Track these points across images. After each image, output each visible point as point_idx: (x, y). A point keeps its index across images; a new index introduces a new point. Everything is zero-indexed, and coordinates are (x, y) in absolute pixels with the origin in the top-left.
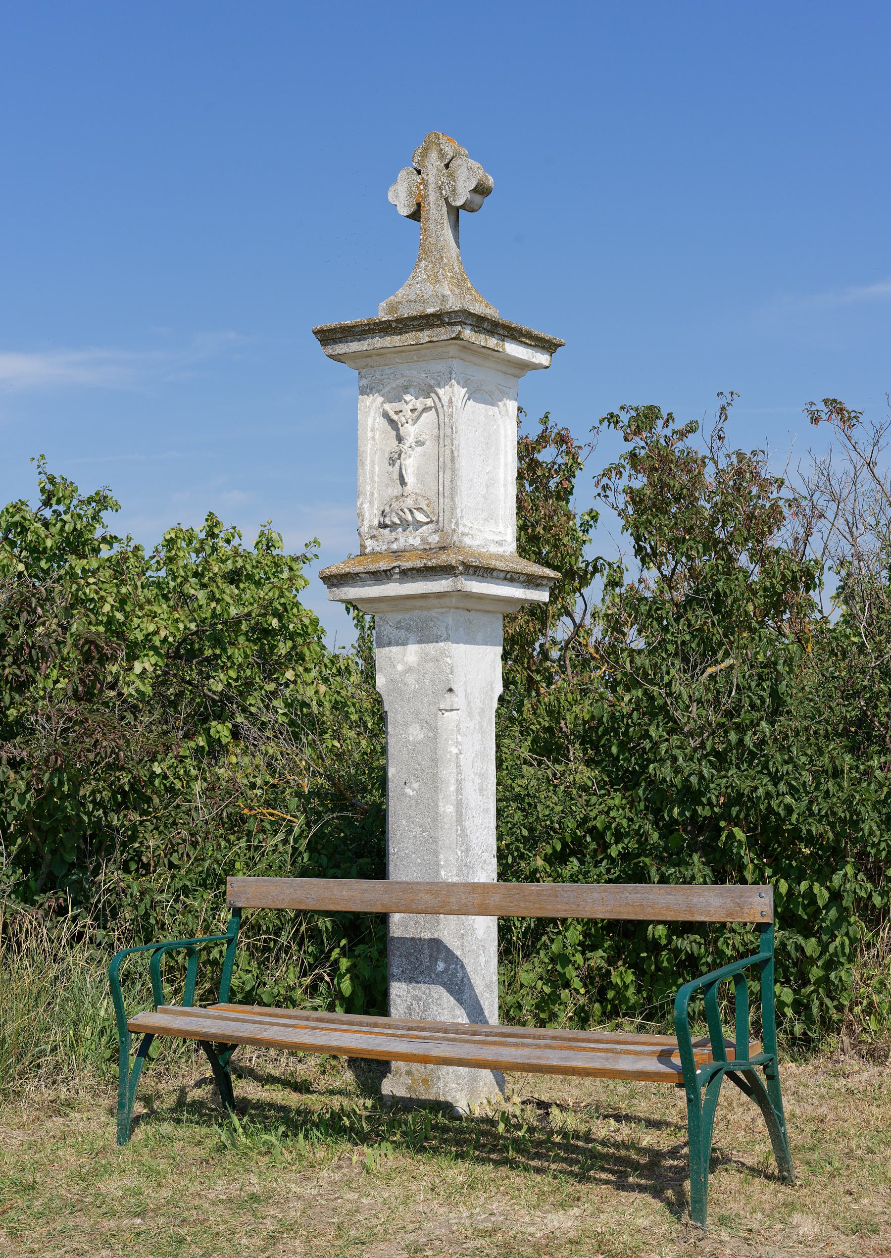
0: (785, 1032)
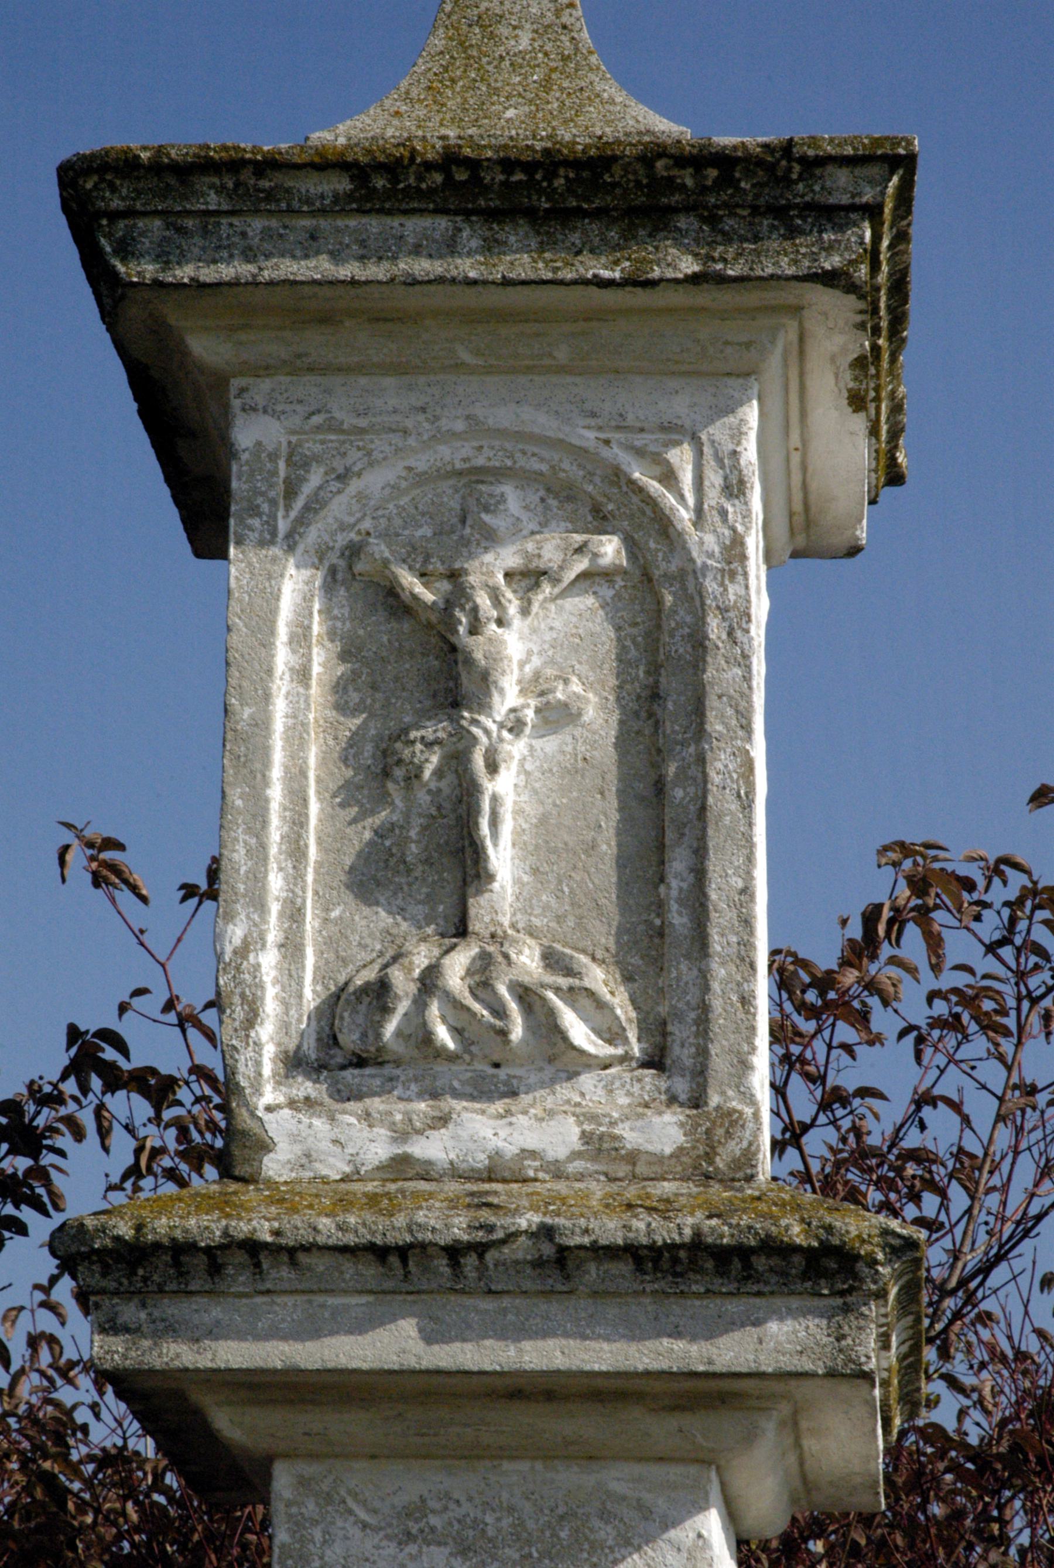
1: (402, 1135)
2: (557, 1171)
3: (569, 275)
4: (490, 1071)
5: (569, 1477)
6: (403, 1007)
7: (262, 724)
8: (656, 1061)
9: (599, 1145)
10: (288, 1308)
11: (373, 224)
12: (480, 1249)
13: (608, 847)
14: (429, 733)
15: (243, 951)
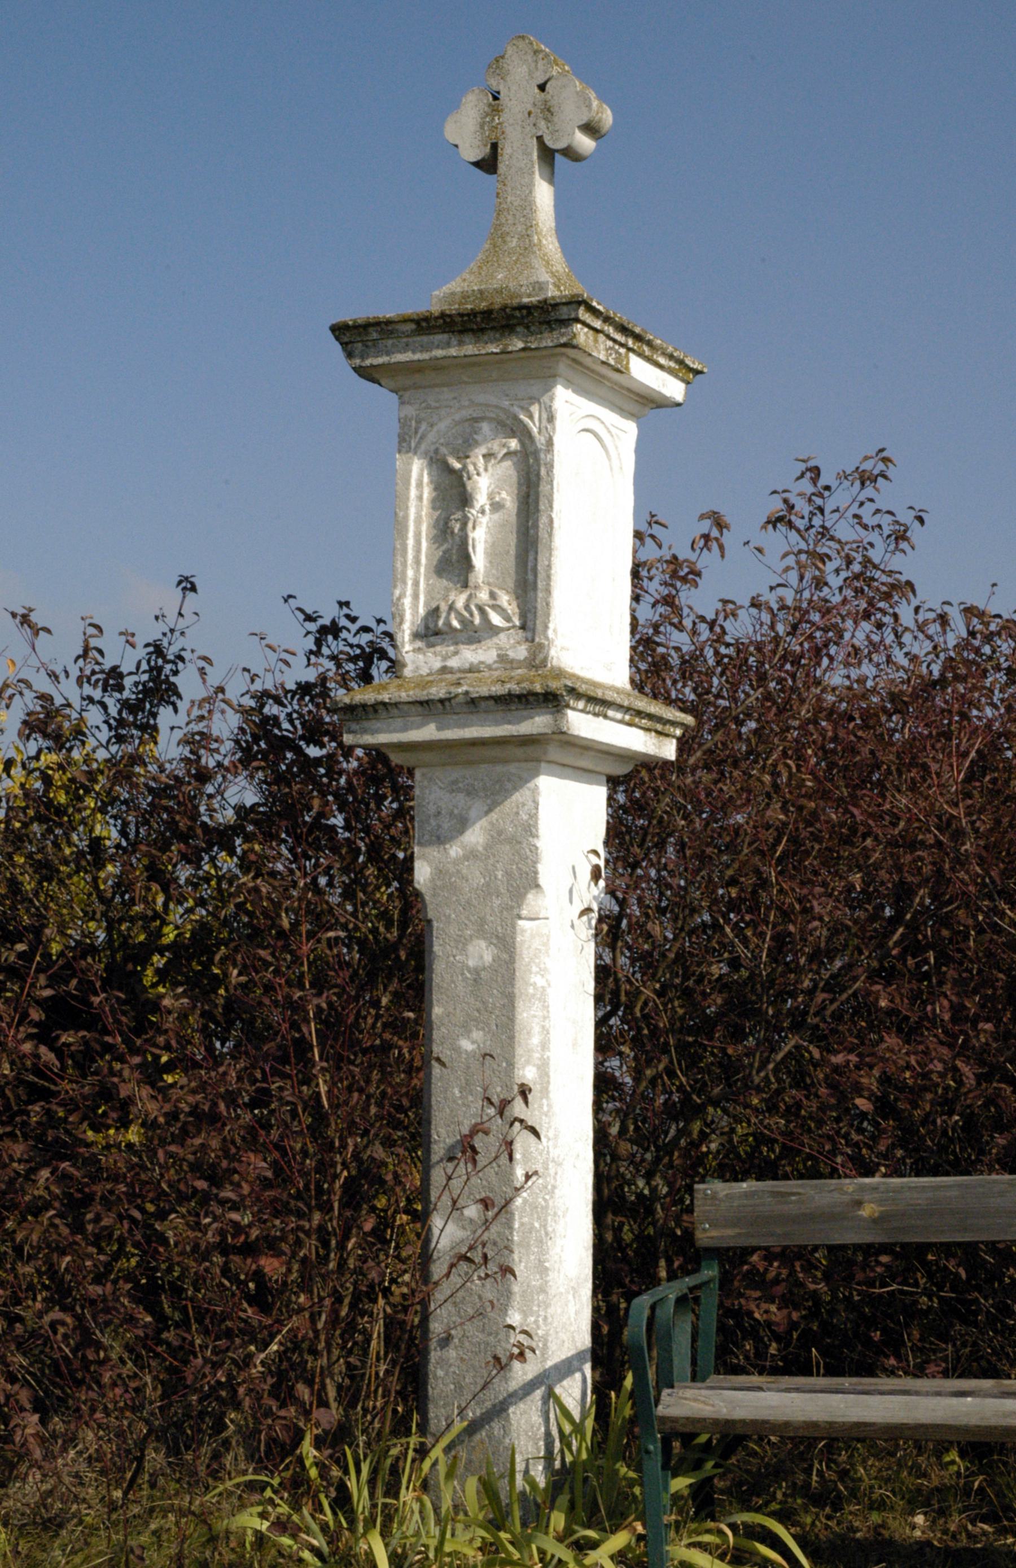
0: (817, 1096)
1: (445, 658)
2: (489, 668)
3: (483, 352)
4: (474, 633)
5: (499, 768)
6: (444, 615)
7: (406, 517)
8: (523, 627)
9: (502, 658)
10: (399, 722)
11: (425, 339)
12: (449, 700)
13: (513, 552)
14: (456, 516)
15: (399, 599)
